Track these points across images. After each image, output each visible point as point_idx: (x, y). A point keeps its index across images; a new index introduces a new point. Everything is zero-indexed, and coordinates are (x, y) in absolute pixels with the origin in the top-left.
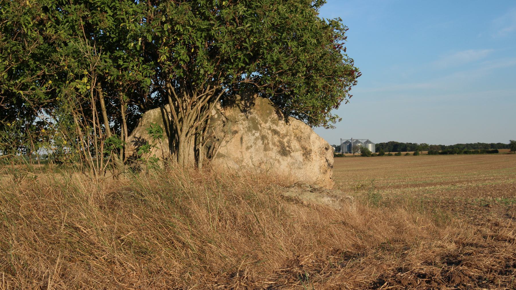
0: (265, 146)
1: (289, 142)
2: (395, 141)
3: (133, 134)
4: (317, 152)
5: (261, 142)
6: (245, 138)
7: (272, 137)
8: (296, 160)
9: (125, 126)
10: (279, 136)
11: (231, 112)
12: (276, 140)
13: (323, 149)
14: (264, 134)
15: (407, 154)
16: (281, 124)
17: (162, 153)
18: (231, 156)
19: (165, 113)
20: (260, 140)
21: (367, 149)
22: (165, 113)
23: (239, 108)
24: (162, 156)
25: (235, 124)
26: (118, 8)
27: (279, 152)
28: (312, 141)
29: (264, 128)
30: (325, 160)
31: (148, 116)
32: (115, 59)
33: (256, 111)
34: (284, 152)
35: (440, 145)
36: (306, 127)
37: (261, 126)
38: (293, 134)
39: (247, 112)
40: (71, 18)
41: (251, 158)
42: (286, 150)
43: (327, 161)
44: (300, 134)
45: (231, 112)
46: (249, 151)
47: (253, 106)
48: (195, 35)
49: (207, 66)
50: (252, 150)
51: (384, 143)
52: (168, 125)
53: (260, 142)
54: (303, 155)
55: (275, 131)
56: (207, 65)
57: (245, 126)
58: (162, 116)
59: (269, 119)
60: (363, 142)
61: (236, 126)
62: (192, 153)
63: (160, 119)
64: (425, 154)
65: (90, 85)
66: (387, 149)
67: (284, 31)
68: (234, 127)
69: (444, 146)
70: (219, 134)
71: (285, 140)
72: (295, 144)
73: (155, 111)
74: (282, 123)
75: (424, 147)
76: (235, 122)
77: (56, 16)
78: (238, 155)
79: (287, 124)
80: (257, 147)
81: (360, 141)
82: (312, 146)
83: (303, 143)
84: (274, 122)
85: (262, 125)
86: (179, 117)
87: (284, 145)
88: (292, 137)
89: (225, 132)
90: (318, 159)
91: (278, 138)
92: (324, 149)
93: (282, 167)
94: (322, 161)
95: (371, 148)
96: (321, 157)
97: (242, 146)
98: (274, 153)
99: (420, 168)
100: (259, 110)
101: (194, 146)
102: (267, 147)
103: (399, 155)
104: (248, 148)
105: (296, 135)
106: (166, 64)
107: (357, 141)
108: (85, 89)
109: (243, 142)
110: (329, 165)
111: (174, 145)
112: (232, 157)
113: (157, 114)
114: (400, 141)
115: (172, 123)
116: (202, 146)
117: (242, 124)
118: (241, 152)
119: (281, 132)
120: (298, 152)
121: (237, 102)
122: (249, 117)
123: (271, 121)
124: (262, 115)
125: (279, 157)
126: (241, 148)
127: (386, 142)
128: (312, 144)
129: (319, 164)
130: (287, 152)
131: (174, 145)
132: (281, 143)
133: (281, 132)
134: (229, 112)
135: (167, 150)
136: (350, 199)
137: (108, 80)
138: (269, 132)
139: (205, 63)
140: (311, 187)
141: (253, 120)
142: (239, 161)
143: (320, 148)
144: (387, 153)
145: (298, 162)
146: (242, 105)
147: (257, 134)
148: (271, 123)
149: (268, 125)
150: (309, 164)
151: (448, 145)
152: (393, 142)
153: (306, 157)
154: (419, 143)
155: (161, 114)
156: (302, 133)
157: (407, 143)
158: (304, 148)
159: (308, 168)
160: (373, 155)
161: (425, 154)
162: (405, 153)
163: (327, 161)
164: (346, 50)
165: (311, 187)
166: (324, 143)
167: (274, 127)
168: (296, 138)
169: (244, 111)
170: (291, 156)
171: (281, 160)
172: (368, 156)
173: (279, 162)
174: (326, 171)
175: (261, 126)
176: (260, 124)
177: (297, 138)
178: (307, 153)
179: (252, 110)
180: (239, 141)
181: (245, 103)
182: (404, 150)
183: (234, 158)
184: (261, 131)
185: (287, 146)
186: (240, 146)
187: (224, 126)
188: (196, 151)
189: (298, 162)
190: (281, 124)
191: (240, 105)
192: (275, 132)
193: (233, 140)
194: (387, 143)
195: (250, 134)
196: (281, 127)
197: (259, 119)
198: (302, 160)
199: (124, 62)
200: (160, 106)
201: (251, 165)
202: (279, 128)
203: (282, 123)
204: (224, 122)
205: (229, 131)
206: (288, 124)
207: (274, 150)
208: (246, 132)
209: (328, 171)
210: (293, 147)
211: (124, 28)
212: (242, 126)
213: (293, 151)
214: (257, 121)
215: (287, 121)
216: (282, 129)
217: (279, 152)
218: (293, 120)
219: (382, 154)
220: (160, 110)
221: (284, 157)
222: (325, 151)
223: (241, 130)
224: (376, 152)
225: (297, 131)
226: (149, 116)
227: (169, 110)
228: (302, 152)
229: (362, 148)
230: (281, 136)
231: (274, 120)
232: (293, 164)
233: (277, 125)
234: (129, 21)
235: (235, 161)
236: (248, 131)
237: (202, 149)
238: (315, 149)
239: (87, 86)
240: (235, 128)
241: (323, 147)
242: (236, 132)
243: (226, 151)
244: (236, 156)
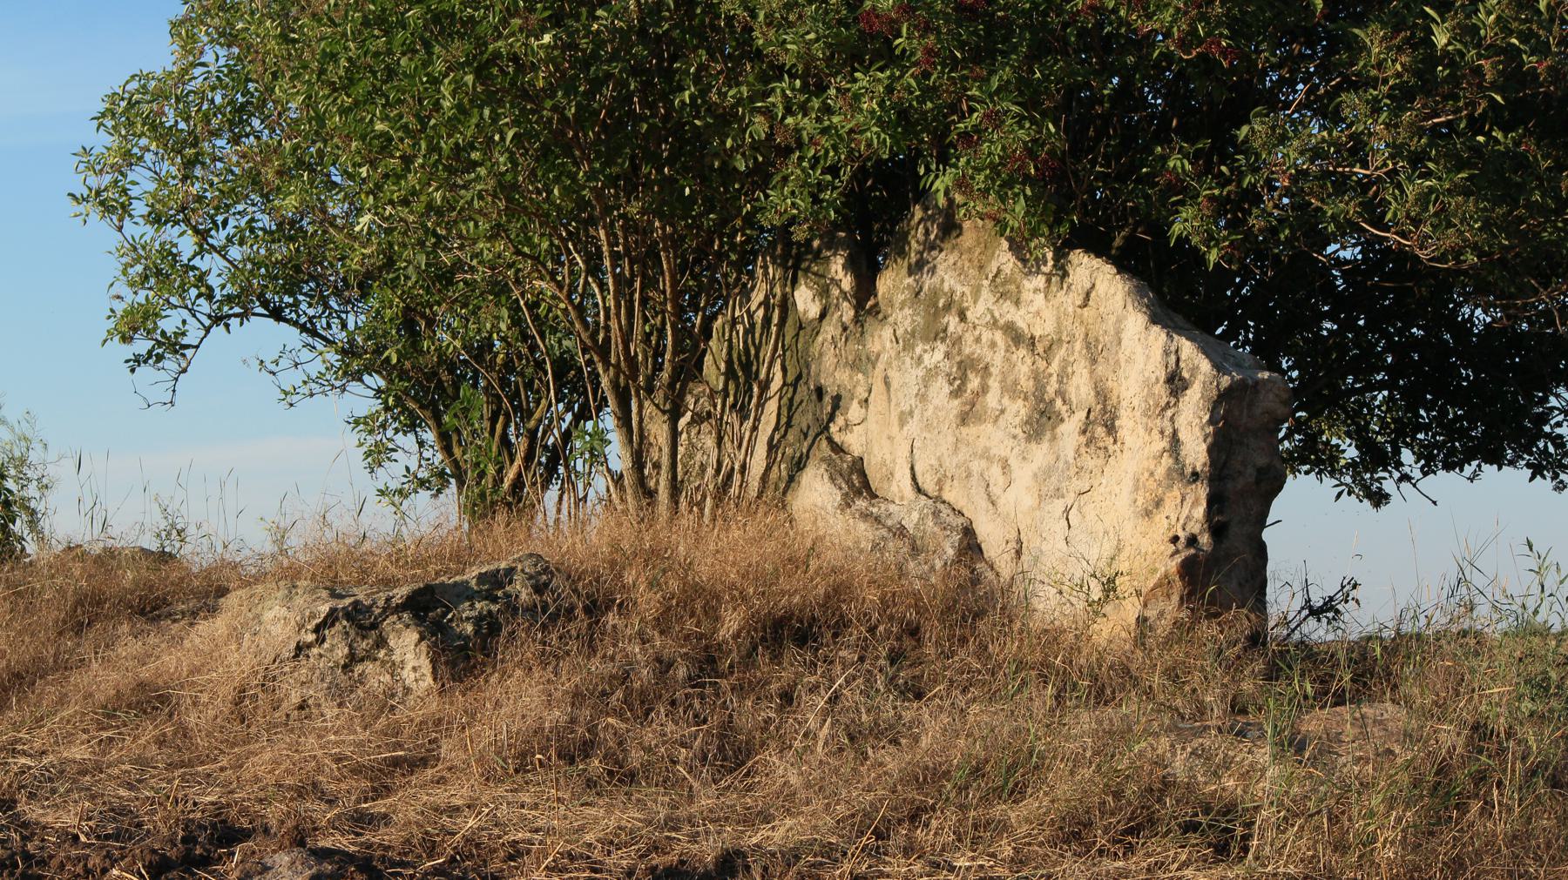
74: (1036, 290)
147: (936, 356)
202: (1022, 312)
215: (1062, 271)
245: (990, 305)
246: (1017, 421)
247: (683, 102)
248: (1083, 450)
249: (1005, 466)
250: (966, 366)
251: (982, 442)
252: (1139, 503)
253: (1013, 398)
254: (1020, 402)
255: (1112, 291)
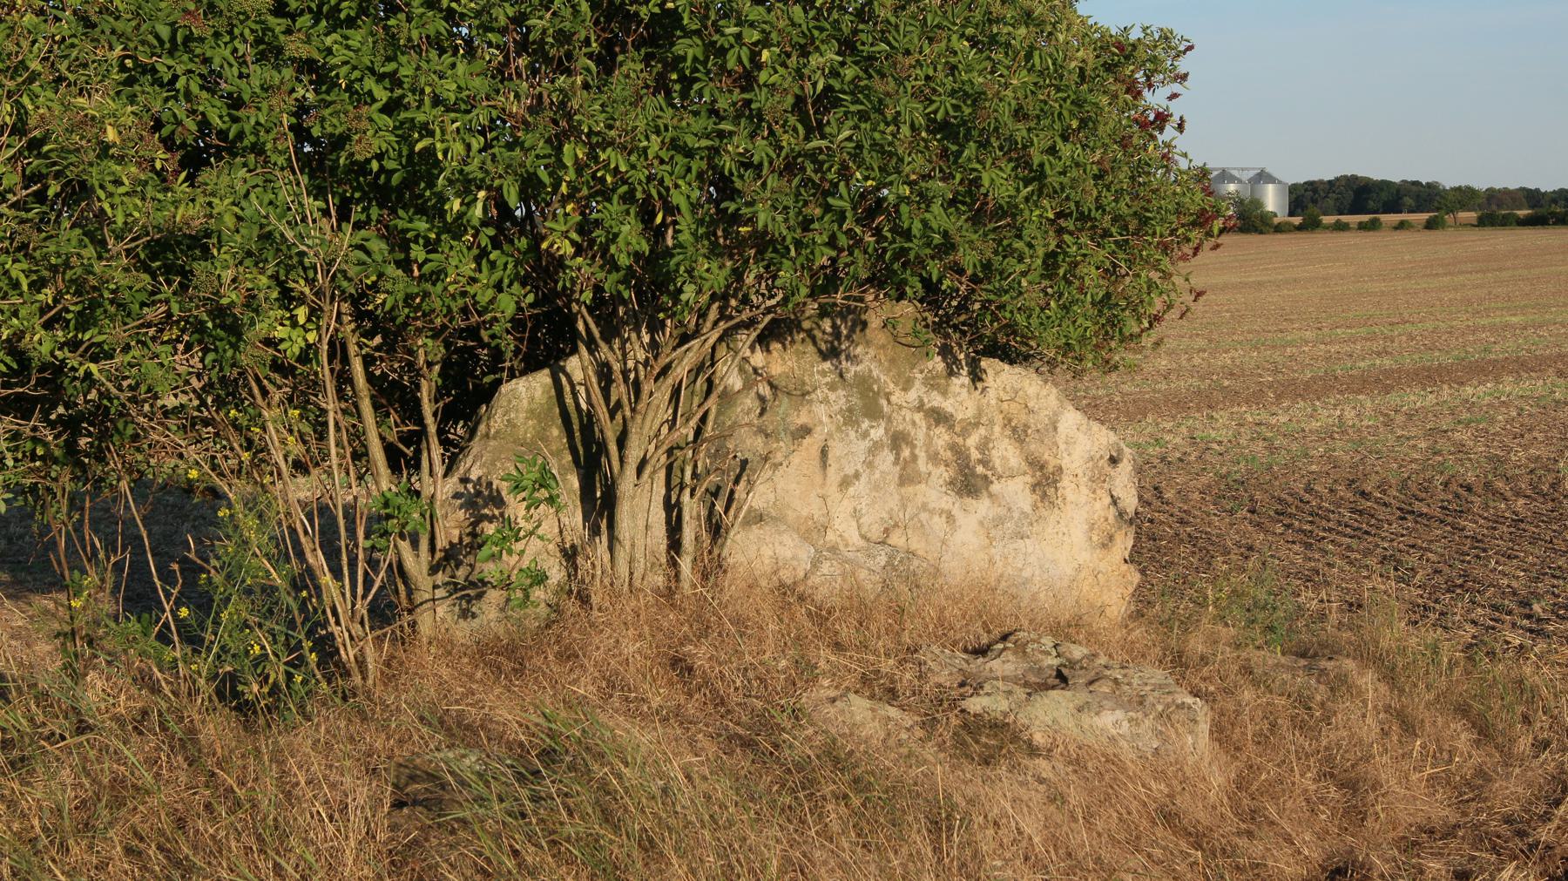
0: (903, 469)
1: (984, 446)
2: (1360, 174)
3: (462, 470)
4: (1080, 475)
5: (891, 458)
6: (836, 450)
7: (928, 435)
8: (1009, 509)
9: (433, 447)
10: (951, 427)
11: (789, 363)
12: (940, 443)
13: (1101, 463)
14: (901, 427)
15: (1401, 226)
16: (957, 389)
17: (557, 530)
18: (789, 512)
19: (567, 389)
20: (886, 451)
21: (1257, 203)
22: (567, 389)
23: (815, 343)
24: (559, 540)
25: (802, 404)
26: (406, 80)
27: (951, 483)
28: (1063, 437)
29: (900, 407)
30: (1108, 500)
31: (510, 401)
32: (400, 242)
33: (872, 352)
34: (969, 482)
35: (1523, 189)
36: (1044, 392)
37: (889, 402)
38: (999, 419)
39: (843, 357)
40: (253, 121)
41: (856, 514)
42: (974, 474)
43: (1115, 501)
44: (1023, 417)
45: (789, 363)
46: (851, 490)
47: (862, 330)
48: (668, 168)
49: (706, 275)
50: (860, 487)
51: (1321, 182)
52: (576, 427)
53: (886, 459)
54: (1034, 488)
55: (938, 413)
56: (708, 270)
57: (836, 408)
58: (555, 400)
59: (919, 376)
60: (1246, 176)
61: (804, 411)
62: (658, 516)
63: (550, 409)
64: (1466, 225)
65: (318, 328)
66: (1331, 202)
67: (968, 138)
68: (798, 416)
69: (1537, 190)
70: (748, 442)
71: (972, 441)
72: (1006, 453)
73: (534, 384)
74: (963, 386)
75: (1465, 197)
76: (802, 394)
77: (201, 109)
78: (815, 509)
79: (976, 388)
80: (877, 475)
81: (1235, 173)
82: (1065, 455)
83: (1033, 447)
84: (932, 383)
85: (893, 399)
86: (619, 417)
87: (968, 457)
88: (997, 429)
89: (767, 436)
90: (1083, 499)
91: (947, 437)
92: (1104, 463)
93: (959, 537)
94: (1098, 505)
95: (1272, 201)
96: (1094, 492)
97: (825, 476)
98: (934, 491)
99: (1446, 279)
100: (883, 347)
101: (663, 491)
102: (909, 470)
103: (1373, 226)
104: (845, 483)
105: (1010, 421)
106: (571, 268)
107: (1225, 176)
108: (300, 340)
109: (829, 462)
110: (1121, 514)
111: (598, 494)
112: (791, 515)
113: (538, 393)
114: (1376, 174)
115: (588, 423)
116: (692, 495)
117: (826, 401)
118: (824, 498)
119: (959, 416)
120: (1017, 480)
121: (806, 325)
122: (848, 376)
123: (926, 382)
124: (892, 361)
125: (948, 501)
126: (824, 484)
127: (1329, 176)
128: (1062, 447)
129: (1086, 516)
130: (980, 482)
131: (598, 494)
132: (959, 452)
133: (959, 416)
134: (780, 362)
135: (575, 518)
136: (1189, 708)
137: (376, 308)
138: (918, 417)
139: (703, 265)
140: (1058, 655)
141: (864, 385)
142: (814, 531)
143: (1092, 459)
144: (1328, 220)
145: (1016, 515)
146: (824, 332)
147: (878, 433)
148: (924, 389)
149: (913, 395)
150: (1053, 518)
151: (1550, 189)
152: (1354, 178)
153: (1044, 496)
154: (1448, 181)
155: (553, 392)
156: (1031, 411)
157: (1404, 182)
158: (1036, 464)
159: (1049, 530)
160: (1279, 229)
161: (1466, 225)
162: (1394, 218)
163: (1115, 501)
164: (1186, 125)
165: (1058, 655)
166: (1105, 443)
167: (936, 400)
168: (1008, 432)
169: (831, 354)
170: (991, 495)
171: (956, 512)
172: (1261, 233)
173: (950, 518)
174: (1111, 538)
175: (889, 402)
176: (888, 396)
177: (1014, 430)
178: (1045, 481)
179: (859, 350)
180: (817, 462)
181: (834, 326)
182: (1393, 206)
183: (798, 517)
184: (890, 420)
185: (980, 461)
186: (818, 479)
187: (763, 412)
188: (672, 510)
189: (1016, 515)
190: (957, 389)
191: (818, 334)
192: (939, 417)
193: (796, 459)
194: (1330, 182)
195: (852, 434)
196: (959, 398)
197: (883, 378)
198: (1028, 508)
199: (428, 252)
200: (549, 366)
201: (854, 538)
202: (951, 400)
203: (963, 386)
204: (762, 399)
205: (781, 428)
206: (979, 385)
207: (934, 478)
208: (839, 429)
209: (1119, 538)
210: (997, 463)
211: (429, 152)
212: (825, 409)
213: (1000, 477)
214: (875, 387)
215: (976, 376)
216: (961, 404)
217: (951, 483)
218: (998, 368)
219: (1311, 225)
220: (548, 380)
221: (969, 501)
222: (1108, 469)
223: (821, 422)
224: (1291, 214)
225: (1013, 405)
226: (514, 403)
227: (578, 376)
228: (1028, 479)
229: (1242, 202)
230: (957, 429)
231: (933, 378)
232: (999, 522)
233: (944, 393)
234: (443, 132)
235: (803, 528)
236: (845, 424)
237: (691, 507)
238: (1074, 466)
239: (307, 331)
240: (803, 419)
241: (1101, 457)
242: (805, 431)
243: (772, 497)
244: (804, 513)
245: (920, 394)
246: (941, 481)
247: (727, 208)
248: (1039, 504)
249: (950, 518)
250: (898, 440)
251: (920, 500)
252: (1095, 538)
253: (936, 465)
254: (943, 468)
255: (1044, 392)
